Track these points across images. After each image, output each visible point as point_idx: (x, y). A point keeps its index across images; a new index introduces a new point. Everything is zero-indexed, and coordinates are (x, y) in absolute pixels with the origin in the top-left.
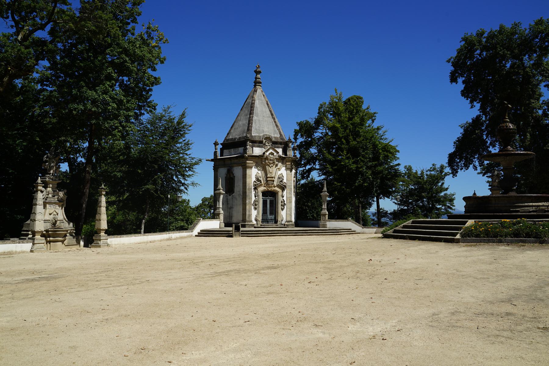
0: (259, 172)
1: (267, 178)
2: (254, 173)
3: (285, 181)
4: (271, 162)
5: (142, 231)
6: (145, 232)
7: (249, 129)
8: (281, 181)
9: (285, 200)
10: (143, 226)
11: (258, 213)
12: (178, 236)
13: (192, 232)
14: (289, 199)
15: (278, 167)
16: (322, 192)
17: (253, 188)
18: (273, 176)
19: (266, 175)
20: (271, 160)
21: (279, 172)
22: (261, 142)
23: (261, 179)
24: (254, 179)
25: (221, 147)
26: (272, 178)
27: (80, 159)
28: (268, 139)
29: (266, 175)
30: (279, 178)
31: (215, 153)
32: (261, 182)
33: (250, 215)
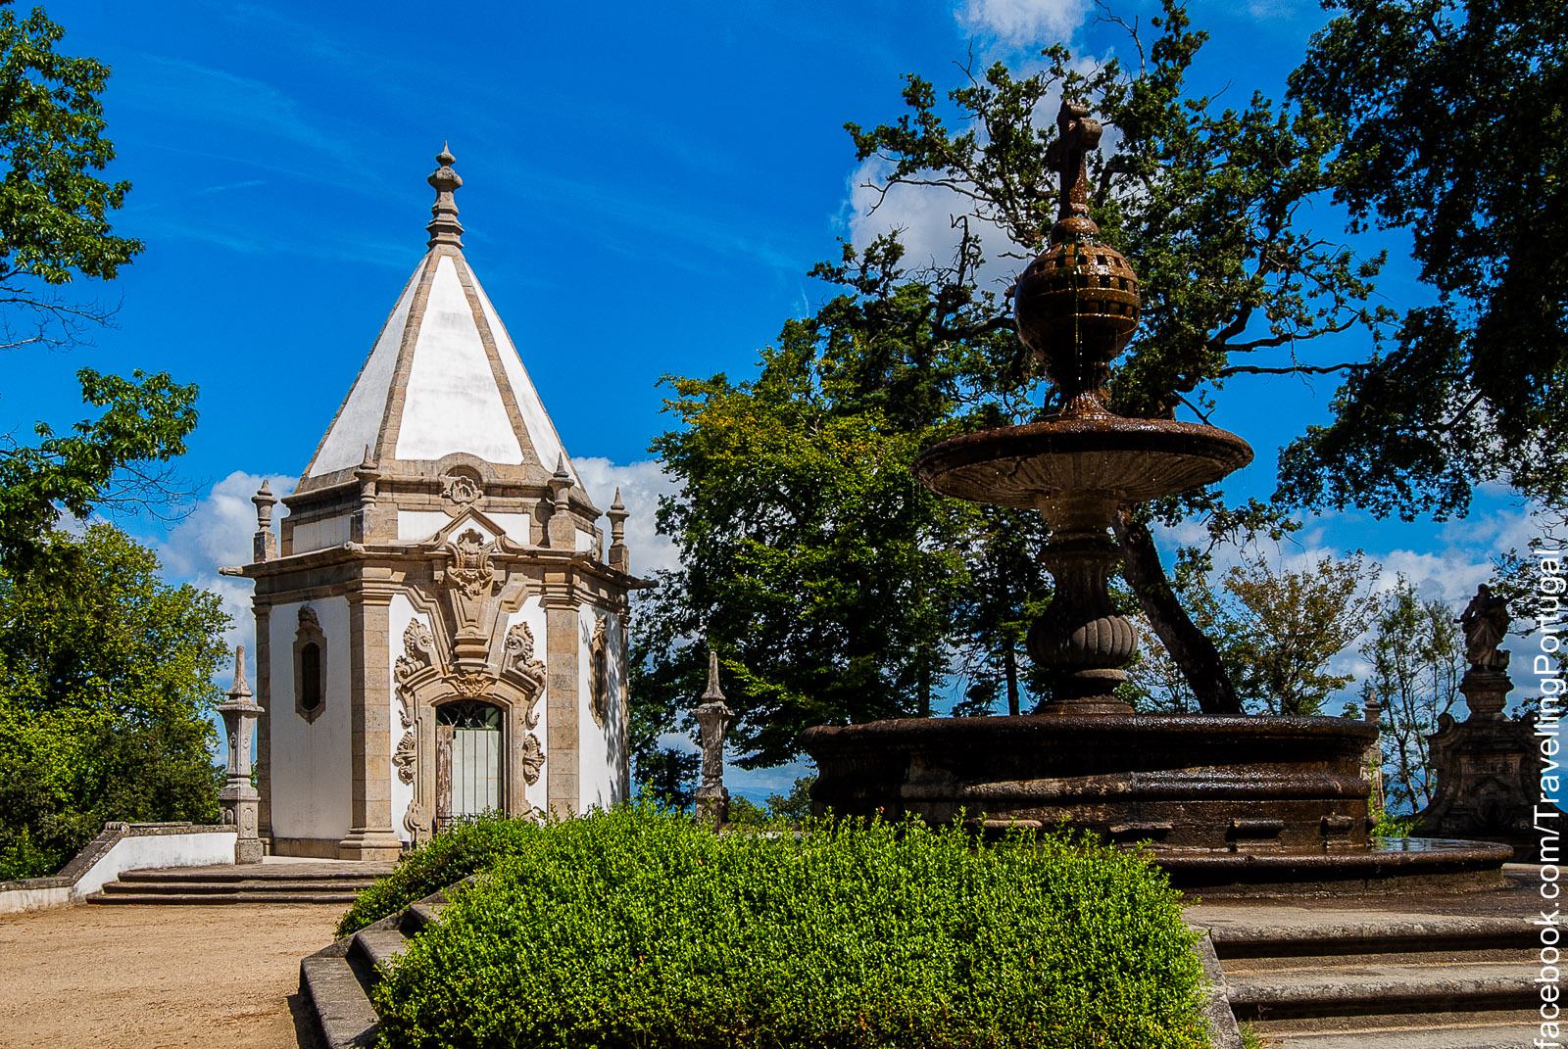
0: (423, 619)
1: (456, 643)
2: (399, 620)
3: (540, 653)
4: (471, 574)
8: (521, 657)
9: (542, 739)
11: (419, 795)
12: (17, 908)
15: (507, 593)
17: (394, 686)
18: (484, 632)
19: (452, 629)
20: (468, 565)
21: (514, 619)
22: (435, 488)
23: (431, 649)
24: (397, 649)
25: (286, 512)
26: (482, 642)
27: (885, 671)
28: (466, 472)
29: (452, 629)
30: (510, 644)
31: (259, 541)
32: (428, 663)
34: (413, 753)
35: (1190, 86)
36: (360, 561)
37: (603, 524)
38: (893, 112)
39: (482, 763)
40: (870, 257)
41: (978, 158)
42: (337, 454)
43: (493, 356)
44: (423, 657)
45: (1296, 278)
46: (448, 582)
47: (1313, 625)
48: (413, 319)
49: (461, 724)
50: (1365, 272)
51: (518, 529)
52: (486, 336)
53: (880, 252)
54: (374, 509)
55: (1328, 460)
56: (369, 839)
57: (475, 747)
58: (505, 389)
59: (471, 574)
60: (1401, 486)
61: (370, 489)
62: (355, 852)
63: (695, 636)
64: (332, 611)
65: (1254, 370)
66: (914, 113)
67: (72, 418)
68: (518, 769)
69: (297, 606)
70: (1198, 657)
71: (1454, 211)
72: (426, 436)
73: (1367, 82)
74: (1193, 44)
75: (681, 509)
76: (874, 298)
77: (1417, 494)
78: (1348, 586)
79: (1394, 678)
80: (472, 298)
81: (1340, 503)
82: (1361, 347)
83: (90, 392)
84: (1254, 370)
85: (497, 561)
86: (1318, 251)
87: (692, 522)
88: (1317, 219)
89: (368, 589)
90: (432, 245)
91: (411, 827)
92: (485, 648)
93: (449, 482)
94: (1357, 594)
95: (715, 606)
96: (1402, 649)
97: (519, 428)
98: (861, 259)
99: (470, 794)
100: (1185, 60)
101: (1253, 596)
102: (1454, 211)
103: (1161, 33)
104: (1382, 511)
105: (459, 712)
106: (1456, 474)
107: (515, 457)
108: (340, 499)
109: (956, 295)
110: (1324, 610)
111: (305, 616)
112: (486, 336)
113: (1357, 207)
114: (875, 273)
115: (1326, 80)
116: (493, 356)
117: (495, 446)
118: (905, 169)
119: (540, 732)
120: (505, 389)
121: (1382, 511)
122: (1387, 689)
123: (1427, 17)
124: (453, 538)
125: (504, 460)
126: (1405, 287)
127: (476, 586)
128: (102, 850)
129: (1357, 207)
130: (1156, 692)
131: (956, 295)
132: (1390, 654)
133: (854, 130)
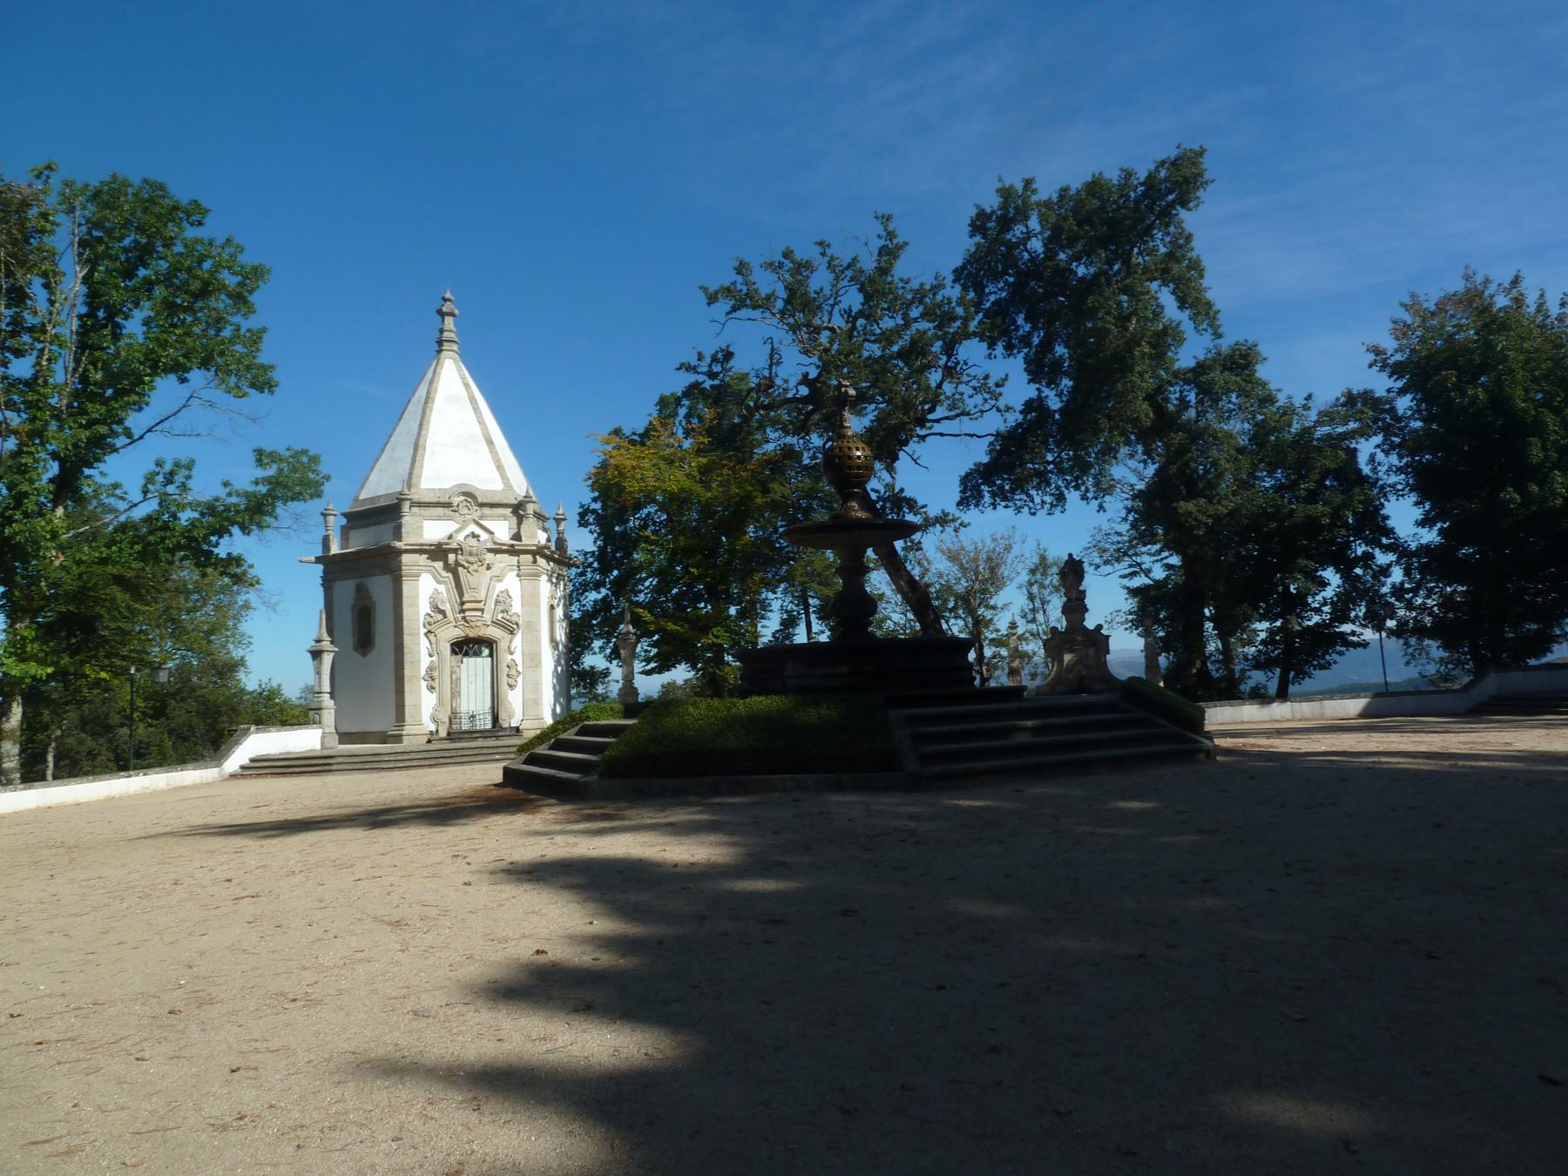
0: (442, 588)
1: (463, 603)
3: (516, 607)
5: (49, 772)
6: (55, 778)
7: (409, 482)
10: (50, 758)
11: (440, 700)
13: (219, 765)
14: (533, 660)
15: (495, 571)
16: (90, 466)
18: (482, 596)
19: (461, 595)
20: (471, 554)
21: (500, 587)
22: (448, 505)
23: (447, 607)
24: (425, 608)
25: (344, 521)
27: (777, 604)
29: (461, 595)
30: (497, 602)
32: (445, 616)
33: (418, 706)
34: (436, 674)
35: (900, 270)
36: (400, 552)
37: (551, 524)
38: (728, 277)
39: (480, 678)
40: (714, 359)
41: (780, 304)
42: (379, 485)
43: (481, 422)
44: (443, 612)
45: (962, 388)
46: (457, 564)
47: (985, 577)
48: (428, 399)
49: (466, 654)
50: (997, 385)
51: (502, 529)
52: (476, 409)
53: (720, 356)
54: (409, 519)
55: (990, 483)
56: (407, 730)
57: (476, 668)
58: (490, 442)
59: (471, 559)
60: (1029, 496)
61: (406, 507)
62: (398, 739)
63: (604, 592)
64: (378, 586)
65: (942, 435)
66: (739, 279)
67: (248, 477)
68: (504, 680)
69: (354, 582)
70: (916, 595)
71: (1047, 346)
72: (435, 476)
73: (996, 276)
74: (900, 247)
75: (594, 512)
76: (716, 382)
77: (1037, 500)
78: (1008, 549)
79: (1038, 604)
80: (466, 385)
81: (994, 506)
82: (994, 423)
83: (259, 462)
84: (942, 435)
85: (490, 550)
86: (972, 371)
87: (600, 520)
88: (972, 351)
89: (405, 570)
90: (440, 352)
91: (435, 720)
92: (480, 605)
93: (456, 500)
94: (1014, 552)
95: (615, 573)
96: (1042, 586)
97: (500, 467)
98: (708, 360)
99: (472, 698)
100: (896, 257)
101: (953, 557)
102: (1047, 346)
103: (882, 242)
104: (1018, 510)
105: (465, 647)
106: (1058, 488)
107: (499, 486)
108: (387, 514)
109: (768, 384)
110: (994, 564)
111: (361, 591)
112: (476, 409)
113: (991, 346)
114: (717, 368)
115: (971, 274)
116: (481, 422)
117: (487, 482)
118: (734, 309)
119: (518, 657)
120: (490, 442)
121: (1018, 510)
122: (1034, 610)
123: (1025, 245)
124: (461, 537)
125: (491, 487)
126: (1019, 390)
127: (475, 567)
128: (237, 743)
129: (991, 346)
130: (896, 617)
131: (768, 384)
132: (1035, 589)
133: (704, 289)
